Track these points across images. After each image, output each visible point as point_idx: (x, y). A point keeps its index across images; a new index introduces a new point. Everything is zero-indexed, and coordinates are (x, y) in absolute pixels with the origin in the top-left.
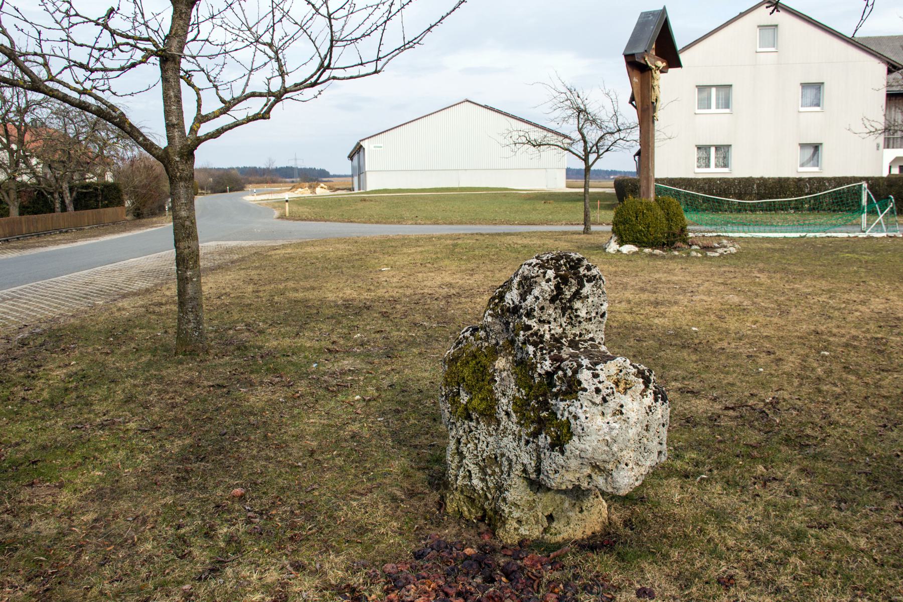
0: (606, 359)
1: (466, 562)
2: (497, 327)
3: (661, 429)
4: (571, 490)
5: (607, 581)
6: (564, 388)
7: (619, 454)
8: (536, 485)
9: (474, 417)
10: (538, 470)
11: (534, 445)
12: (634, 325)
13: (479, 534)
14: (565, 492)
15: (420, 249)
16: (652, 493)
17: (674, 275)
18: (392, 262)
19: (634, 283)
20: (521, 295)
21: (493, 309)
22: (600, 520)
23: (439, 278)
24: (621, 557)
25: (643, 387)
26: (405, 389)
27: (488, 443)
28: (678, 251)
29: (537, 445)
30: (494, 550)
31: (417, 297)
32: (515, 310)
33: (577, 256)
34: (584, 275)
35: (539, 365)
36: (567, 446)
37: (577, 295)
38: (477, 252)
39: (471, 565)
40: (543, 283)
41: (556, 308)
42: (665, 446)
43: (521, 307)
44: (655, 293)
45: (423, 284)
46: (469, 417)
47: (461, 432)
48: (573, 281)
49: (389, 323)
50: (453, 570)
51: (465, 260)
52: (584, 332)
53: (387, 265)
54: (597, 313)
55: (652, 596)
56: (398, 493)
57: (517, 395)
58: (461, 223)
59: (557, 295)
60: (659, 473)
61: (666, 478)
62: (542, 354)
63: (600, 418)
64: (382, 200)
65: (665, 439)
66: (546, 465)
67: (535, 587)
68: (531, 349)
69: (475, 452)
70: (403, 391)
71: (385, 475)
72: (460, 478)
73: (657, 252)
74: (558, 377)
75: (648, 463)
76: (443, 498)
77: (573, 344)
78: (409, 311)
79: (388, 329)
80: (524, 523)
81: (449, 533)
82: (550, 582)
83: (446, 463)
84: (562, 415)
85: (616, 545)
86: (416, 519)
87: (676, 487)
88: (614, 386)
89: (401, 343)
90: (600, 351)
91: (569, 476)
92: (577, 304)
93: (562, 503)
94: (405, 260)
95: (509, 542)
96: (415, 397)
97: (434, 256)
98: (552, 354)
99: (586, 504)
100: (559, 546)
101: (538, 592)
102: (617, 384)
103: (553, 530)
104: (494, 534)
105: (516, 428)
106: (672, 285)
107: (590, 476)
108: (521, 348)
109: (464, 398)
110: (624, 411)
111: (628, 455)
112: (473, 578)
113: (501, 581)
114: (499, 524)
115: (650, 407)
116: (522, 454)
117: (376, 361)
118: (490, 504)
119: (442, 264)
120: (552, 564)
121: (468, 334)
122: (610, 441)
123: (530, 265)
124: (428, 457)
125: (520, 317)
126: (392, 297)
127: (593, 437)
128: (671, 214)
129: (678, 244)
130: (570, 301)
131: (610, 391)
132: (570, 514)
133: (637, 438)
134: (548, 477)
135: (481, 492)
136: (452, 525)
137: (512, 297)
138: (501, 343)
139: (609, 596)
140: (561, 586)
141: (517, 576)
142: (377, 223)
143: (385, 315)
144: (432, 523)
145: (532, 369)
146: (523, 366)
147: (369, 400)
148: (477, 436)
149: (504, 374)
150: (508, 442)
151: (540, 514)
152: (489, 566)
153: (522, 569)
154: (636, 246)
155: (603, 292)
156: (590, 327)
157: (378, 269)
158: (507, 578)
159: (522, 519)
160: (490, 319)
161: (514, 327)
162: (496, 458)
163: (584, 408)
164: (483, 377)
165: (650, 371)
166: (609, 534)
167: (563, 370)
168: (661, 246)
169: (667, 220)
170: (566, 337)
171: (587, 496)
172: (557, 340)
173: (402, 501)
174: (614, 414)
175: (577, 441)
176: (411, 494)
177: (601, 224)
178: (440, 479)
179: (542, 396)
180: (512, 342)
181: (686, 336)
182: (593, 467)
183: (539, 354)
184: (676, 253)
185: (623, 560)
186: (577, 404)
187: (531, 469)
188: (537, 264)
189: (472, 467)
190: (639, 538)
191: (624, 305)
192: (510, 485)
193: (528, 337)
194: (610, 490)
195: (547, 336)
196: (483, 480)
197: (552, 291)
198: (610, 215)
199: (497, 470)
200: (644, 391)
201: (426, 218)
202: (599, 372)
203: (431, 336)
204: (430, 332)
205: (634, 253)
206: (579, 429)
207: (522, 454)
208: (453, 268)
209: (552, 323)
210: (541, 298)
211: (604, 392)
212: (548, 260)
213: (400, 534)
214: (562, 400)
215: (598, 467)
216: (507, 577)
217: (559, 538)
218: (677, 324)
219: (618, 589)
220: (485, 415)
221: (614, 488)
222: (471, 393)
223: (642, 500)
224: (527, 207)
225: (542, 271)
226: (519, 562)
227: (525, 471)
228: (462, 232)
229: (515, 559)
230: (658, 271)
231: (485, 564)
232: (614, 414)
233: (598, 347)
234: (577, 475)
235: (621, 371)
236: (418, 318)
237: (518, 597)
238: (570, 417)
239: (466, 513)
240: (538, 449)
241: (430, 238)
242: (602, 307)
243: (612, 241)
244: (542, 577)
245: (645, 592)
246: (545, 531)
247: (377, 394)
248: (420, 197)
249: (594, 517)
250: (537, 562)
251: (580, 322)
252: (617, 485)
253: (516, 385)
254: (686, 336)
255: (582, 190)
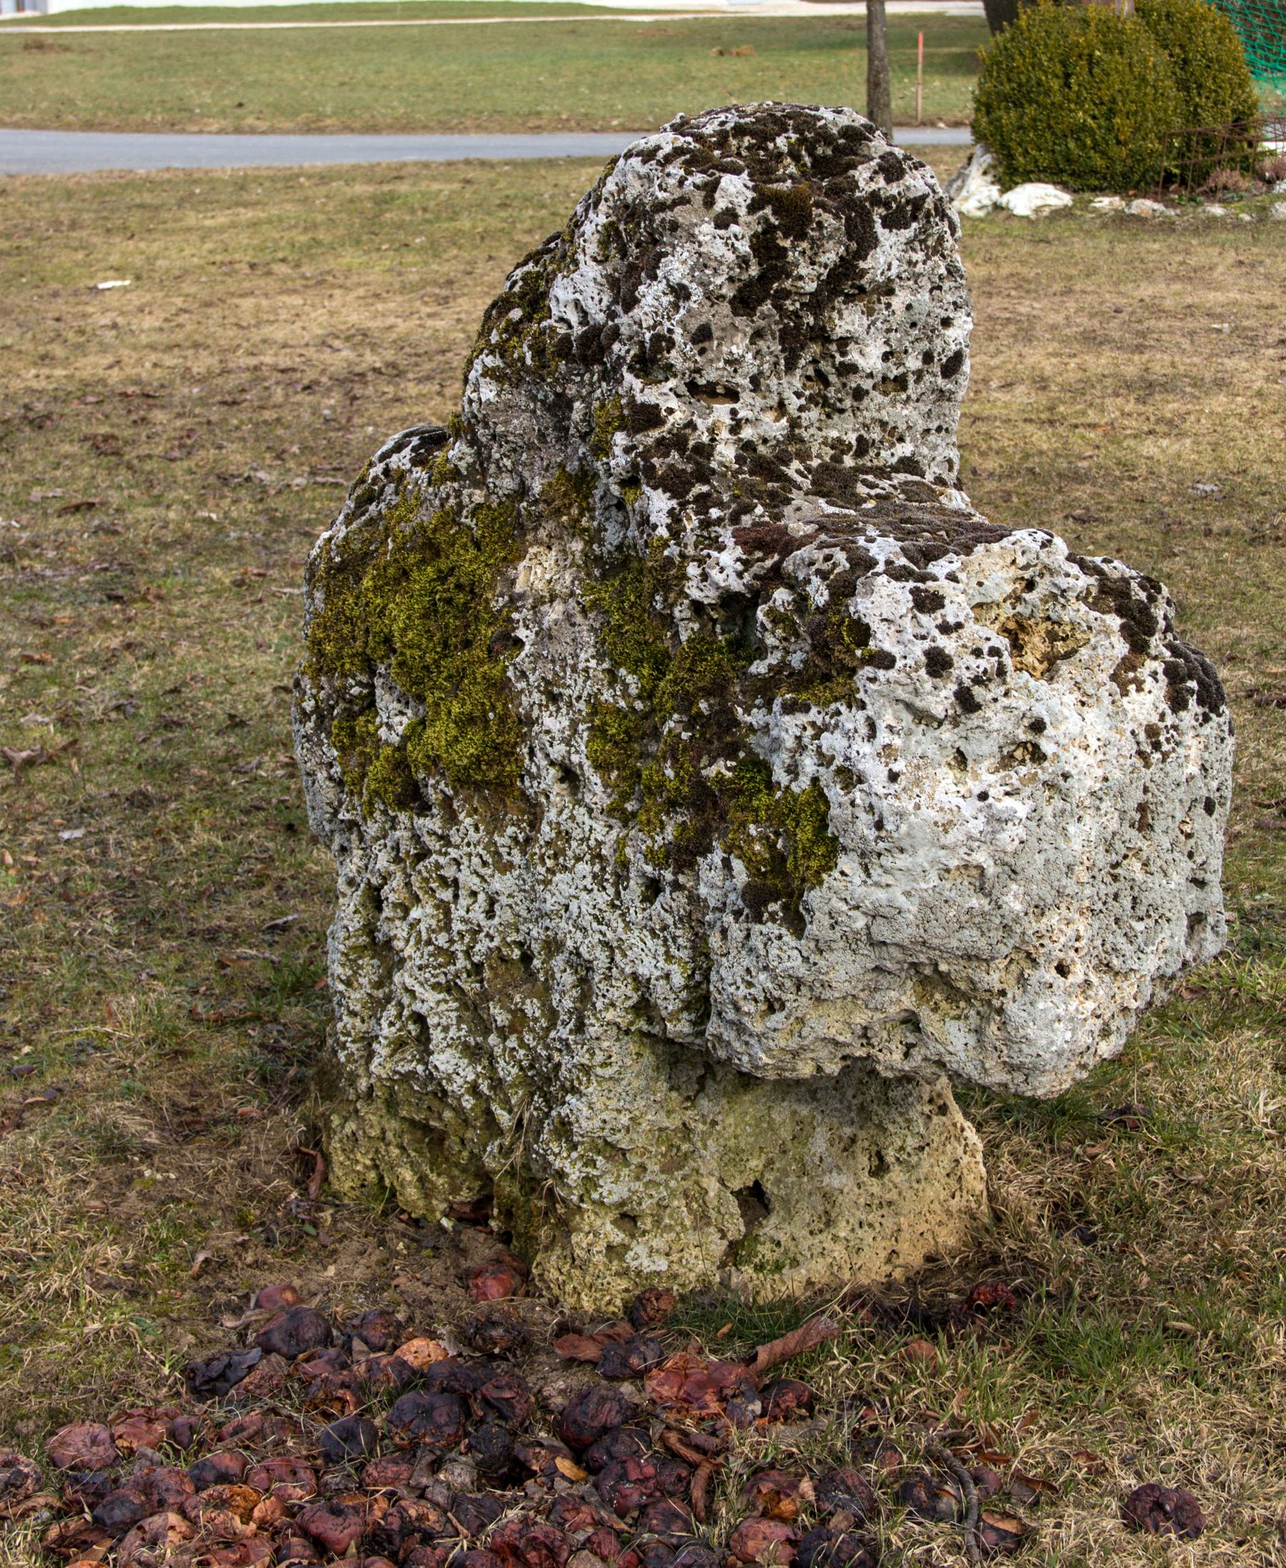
0: (967, 536)
1: (407, 1398)
2: (519, 422)
3: (1200, 822)
4: (837, 1083)
5: (995, 1459)
6: (796, 660)
7: (1031, 925)
8: (692, 1062)
9: (433, 796)
10: (700, 1003)
11: (681, 898)
12: (1063, 464)
13: (465, 1278)
14: (809, 1089)
15: (247, 215)
16: (1160, 1088)
17: (1210, 286)
18: (138, 261)
19: (1059, 319)
20: (613, 283)
21: (501, 350)
22: (955, 1204)
23: (320, 315)
24: (1051, 1357)
25: (1122, 648)
26: (174, 715)
27: (492, 901)
28: (1223, 201)
29: (694, 899)
30: (524, 1343)
31: (232, 382)
32: (592, 347)
33: (844, 121)
34: (875, 198)
35: (693, 570)
36: (814, 897)
37: (844, 281)
38: (465, 223)
39: (428, 1411)
40: (706, 230)
41: (758, 335)
42: (1216, 894)
43: (615, 334)
44: (1140, 349)
45: (256, 336)
46: (413, 798)
47: (383, 861)
48: (828, 219)
49: (122, 476)
50: (349, 1435)
51: (421, 250)
52: (876, 434)
53: (119, 271)
54: (928, 357)
55: (1190, 1526)
56: (133, 1124)
57: (607, 696)
58: (406, 126)
59: (764, 280)
60: (1190, 1009)
61: (1212, 1031)
62: (706, 524)
63: (947, 777)
64: (108, 45)
65: (1216, 863)
66: (730, 976)
67: (697, 1493)
68: (659, 504)
69: (442, 940)
70: (169, 725)
71: (79, 1055)
72: (381, 1049)
73: (1144, 206)
74: (771, 613)
75: (1151, 964)
76: (316, 1132)
77: (832, 482)
78: (202, 432)
79: (115, 498)
80: (647, 1223)
81: (338, 1279)
82: (757, 1472)
83: (326, 996)
84: (793, 770)
85: (1029, 1309)
86: (201, 1225)
87: (1255, 1066)
88: (1002, 642)
89: (165, 546)
90: (942, 510)
91: (828, 1023)
92: (848, 320)
93: (802, 1134)
94: (192, 253)
95: (587, 1304)
96: (217, 745)
97: (303, 238)
98: (746, 520)
99: (899, 1140)
100: (792, 1314)
101: (711, 1517)
102: (1016, 634)
103: (765, 1251)
104: (524, 1278)
105: (603, 833)
106: (1205, 321)
107: (911, 1021)
108: (620, 505)
109: (392, 720)
110: (1047, 747)
111: (1068, 929)
112: (436, 1466)
113: (552, 1473)
114: (544, 1233)
115: (1152, 731)
116: (633, 938)
117: (64, 615)
118: (505, 1152)
119: (332, 263)
120: (763, 1392)
121: (401, 460)
122: (991, 870)
123: (648, 155)
124: (265, 976)
125: (611, 375)
126: (137, 382)
127: (923, 857)
128: (1198, 62)
129: (1225, 176)
130: (817, 303)
131: (987, 663)
132: (835, 1181)
133: (1102, 859)
134: (740, 1029)
135: (468, 1102)
136: (354, 1245)
137: (579, 292)
138: (537, 486)
139: (1010, 1526)
140: (806, 1486)
141: (619, 1449)
142: (88, 126)
143: (104, 447)
144: (269, 1242)
145: (665, 586)
146: (629, 581)
147: (30, 763)
148: (449, 872)
149: (553, 613)
150: (574, 890)
151: (712, 1186)
152: (499, 1409)
153: (637, 1417)
154: (1065, 186)
155: (952, 271)
156: (903, 414)
157: (84, 283)
158: (577, 1460)
159: (641, 1219)
160: (488, 392)
161: (587, 418)
162: (527, 958)
163: (883, 737)
164: (467, 627)
165: (1151, 585)
166: (995, 1259)
167: (792, 584)
168: (1161, 185)
169: (1183, 85)
170: (804, 456)
171: (902, 1105)
172: (764, 467)
173: (148, 1154)
174: (1007, 761)
175: (857, 876)
176: (188, 1124)
177: (929, 123)
178: (307, 1059)
179: (707, 693)
180: (583, 481)
181: (1264, 501)
182: (924, 981)
183: (691, 523)
184: (1217, 210)
185: (1060, 1370)
186: (853, 719)
187: (668, 1000)
188: (678, 151)
189: (429, 1000)
190: (1119, 1278)
191: (1022, 395)
192: (586, 1070)
193: (646, 455)
194: (998, 1076)
195: (726, 452)
196: (473, 1053)
197: (743, 262)
198: (962, 92)
199: (532, 1008)
200: (1128, 664)
201: (277, 109)
202: (944, 587)
203: (284, 521)
204: (281, 505)
205: (1059, 214)
206: (864, 825)
207: (633, 938)
208: (376, 275)
209: (746, 396)
210: (697, 292)
211: (965, 667)
212: (723, 137)
213: (132, 1294)
214: (789, 709)
215: (945, 979)
216: (579, 1455)
217: (792, 1283)
218: (1230, 457)
219: (1043, 1489)
220: (478, 786)
221: (1012, 1068)
222: (421, 699)
223: (1125, 1120)
224: (654, 68)
225: (699, 178)
226: (626, 1388)
227: (644, 1007)
228: (410, 158)
229: (612, 1378)
230: (1148, 275)
231: (486, 1402)
232: (1007, 761)
233: (934, 496)
234: (860, 1018)
235: (1030, 586)
236: (236, 457)
237: (624, 1540)
238: (826, 775)
239: (412, 1193)
240: (695, 917)
241: (288, 181)
242: (951, 333)
243: (975, 171)
244: (725, 1449)
245: (1159, 1506)
246: (736, 1253)
247: (61, 740)
248: (254, 38)
249: (936, 1190)
250: (702, 1386)
251: (859, 394)
252: (1025, 1055)
253: (600, 657)
254: (1264, 501)
255: (860, 9)
